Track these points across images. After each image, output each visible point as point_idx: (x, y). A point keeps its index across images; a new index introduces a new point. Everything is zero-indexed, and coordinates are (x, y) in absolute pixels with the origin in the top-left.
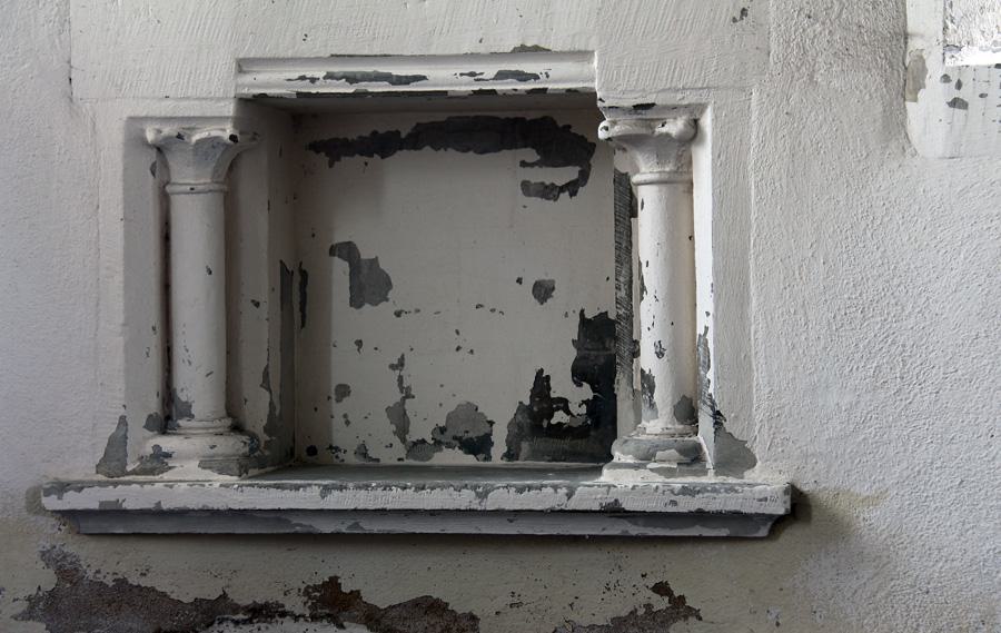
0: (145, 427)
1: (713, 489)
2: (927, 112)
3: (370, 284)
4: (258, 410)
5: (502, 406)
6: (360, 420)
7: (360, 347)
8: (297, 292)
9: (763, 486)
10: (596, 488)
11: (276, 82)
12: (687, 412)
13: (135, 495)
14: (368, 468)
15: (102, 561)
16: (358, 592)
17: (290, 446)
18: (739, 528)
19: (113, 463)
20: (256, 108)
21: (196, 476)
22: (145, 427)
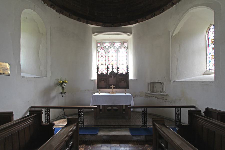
0: (13, 112)
1: (164, 94)
2: (171, 83)
3: (156, 87)
4: (152, 91)
5: (160, 91)
6: (155, 91)
7: (155, 89)
8: (153, 87)
9: (166, 94)
10: (162, 94)
11: (152, 82)
12: (164, 92)
13: (147, 93)
14: (155, 93)
15: (147, 95)
16: (97, 89)
17: (153, 92)
18: (165, 95)
19: (147, 92)
20: (151, 82)
21: (149, 93)
22: (13, 112)
